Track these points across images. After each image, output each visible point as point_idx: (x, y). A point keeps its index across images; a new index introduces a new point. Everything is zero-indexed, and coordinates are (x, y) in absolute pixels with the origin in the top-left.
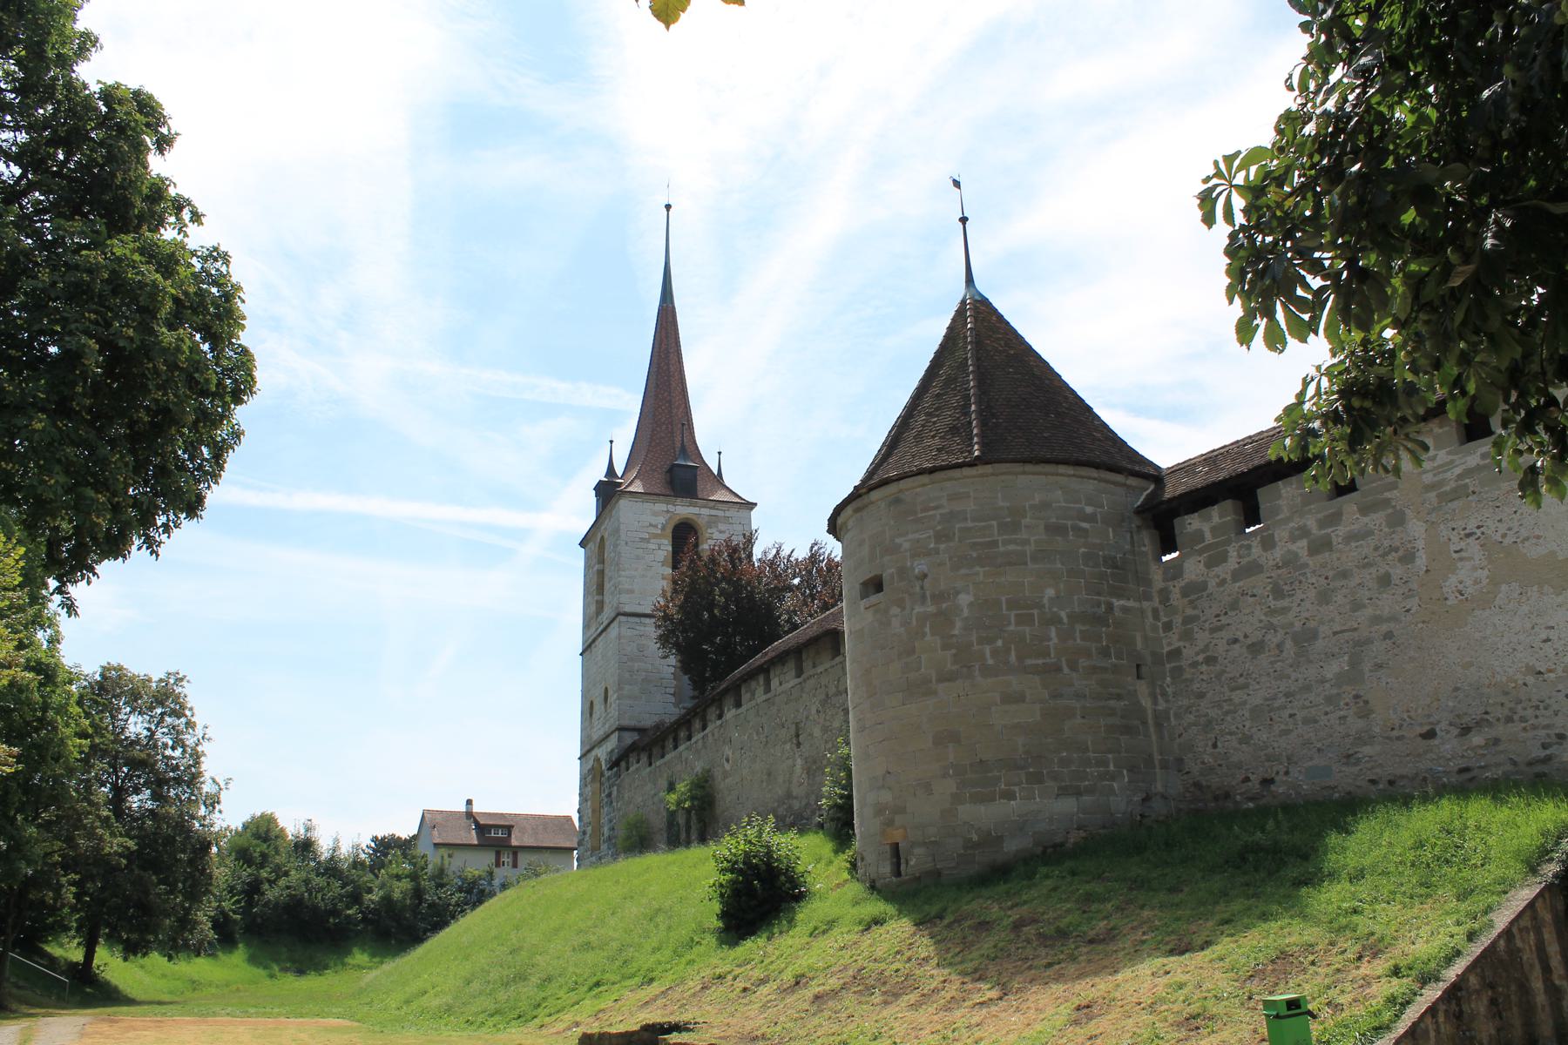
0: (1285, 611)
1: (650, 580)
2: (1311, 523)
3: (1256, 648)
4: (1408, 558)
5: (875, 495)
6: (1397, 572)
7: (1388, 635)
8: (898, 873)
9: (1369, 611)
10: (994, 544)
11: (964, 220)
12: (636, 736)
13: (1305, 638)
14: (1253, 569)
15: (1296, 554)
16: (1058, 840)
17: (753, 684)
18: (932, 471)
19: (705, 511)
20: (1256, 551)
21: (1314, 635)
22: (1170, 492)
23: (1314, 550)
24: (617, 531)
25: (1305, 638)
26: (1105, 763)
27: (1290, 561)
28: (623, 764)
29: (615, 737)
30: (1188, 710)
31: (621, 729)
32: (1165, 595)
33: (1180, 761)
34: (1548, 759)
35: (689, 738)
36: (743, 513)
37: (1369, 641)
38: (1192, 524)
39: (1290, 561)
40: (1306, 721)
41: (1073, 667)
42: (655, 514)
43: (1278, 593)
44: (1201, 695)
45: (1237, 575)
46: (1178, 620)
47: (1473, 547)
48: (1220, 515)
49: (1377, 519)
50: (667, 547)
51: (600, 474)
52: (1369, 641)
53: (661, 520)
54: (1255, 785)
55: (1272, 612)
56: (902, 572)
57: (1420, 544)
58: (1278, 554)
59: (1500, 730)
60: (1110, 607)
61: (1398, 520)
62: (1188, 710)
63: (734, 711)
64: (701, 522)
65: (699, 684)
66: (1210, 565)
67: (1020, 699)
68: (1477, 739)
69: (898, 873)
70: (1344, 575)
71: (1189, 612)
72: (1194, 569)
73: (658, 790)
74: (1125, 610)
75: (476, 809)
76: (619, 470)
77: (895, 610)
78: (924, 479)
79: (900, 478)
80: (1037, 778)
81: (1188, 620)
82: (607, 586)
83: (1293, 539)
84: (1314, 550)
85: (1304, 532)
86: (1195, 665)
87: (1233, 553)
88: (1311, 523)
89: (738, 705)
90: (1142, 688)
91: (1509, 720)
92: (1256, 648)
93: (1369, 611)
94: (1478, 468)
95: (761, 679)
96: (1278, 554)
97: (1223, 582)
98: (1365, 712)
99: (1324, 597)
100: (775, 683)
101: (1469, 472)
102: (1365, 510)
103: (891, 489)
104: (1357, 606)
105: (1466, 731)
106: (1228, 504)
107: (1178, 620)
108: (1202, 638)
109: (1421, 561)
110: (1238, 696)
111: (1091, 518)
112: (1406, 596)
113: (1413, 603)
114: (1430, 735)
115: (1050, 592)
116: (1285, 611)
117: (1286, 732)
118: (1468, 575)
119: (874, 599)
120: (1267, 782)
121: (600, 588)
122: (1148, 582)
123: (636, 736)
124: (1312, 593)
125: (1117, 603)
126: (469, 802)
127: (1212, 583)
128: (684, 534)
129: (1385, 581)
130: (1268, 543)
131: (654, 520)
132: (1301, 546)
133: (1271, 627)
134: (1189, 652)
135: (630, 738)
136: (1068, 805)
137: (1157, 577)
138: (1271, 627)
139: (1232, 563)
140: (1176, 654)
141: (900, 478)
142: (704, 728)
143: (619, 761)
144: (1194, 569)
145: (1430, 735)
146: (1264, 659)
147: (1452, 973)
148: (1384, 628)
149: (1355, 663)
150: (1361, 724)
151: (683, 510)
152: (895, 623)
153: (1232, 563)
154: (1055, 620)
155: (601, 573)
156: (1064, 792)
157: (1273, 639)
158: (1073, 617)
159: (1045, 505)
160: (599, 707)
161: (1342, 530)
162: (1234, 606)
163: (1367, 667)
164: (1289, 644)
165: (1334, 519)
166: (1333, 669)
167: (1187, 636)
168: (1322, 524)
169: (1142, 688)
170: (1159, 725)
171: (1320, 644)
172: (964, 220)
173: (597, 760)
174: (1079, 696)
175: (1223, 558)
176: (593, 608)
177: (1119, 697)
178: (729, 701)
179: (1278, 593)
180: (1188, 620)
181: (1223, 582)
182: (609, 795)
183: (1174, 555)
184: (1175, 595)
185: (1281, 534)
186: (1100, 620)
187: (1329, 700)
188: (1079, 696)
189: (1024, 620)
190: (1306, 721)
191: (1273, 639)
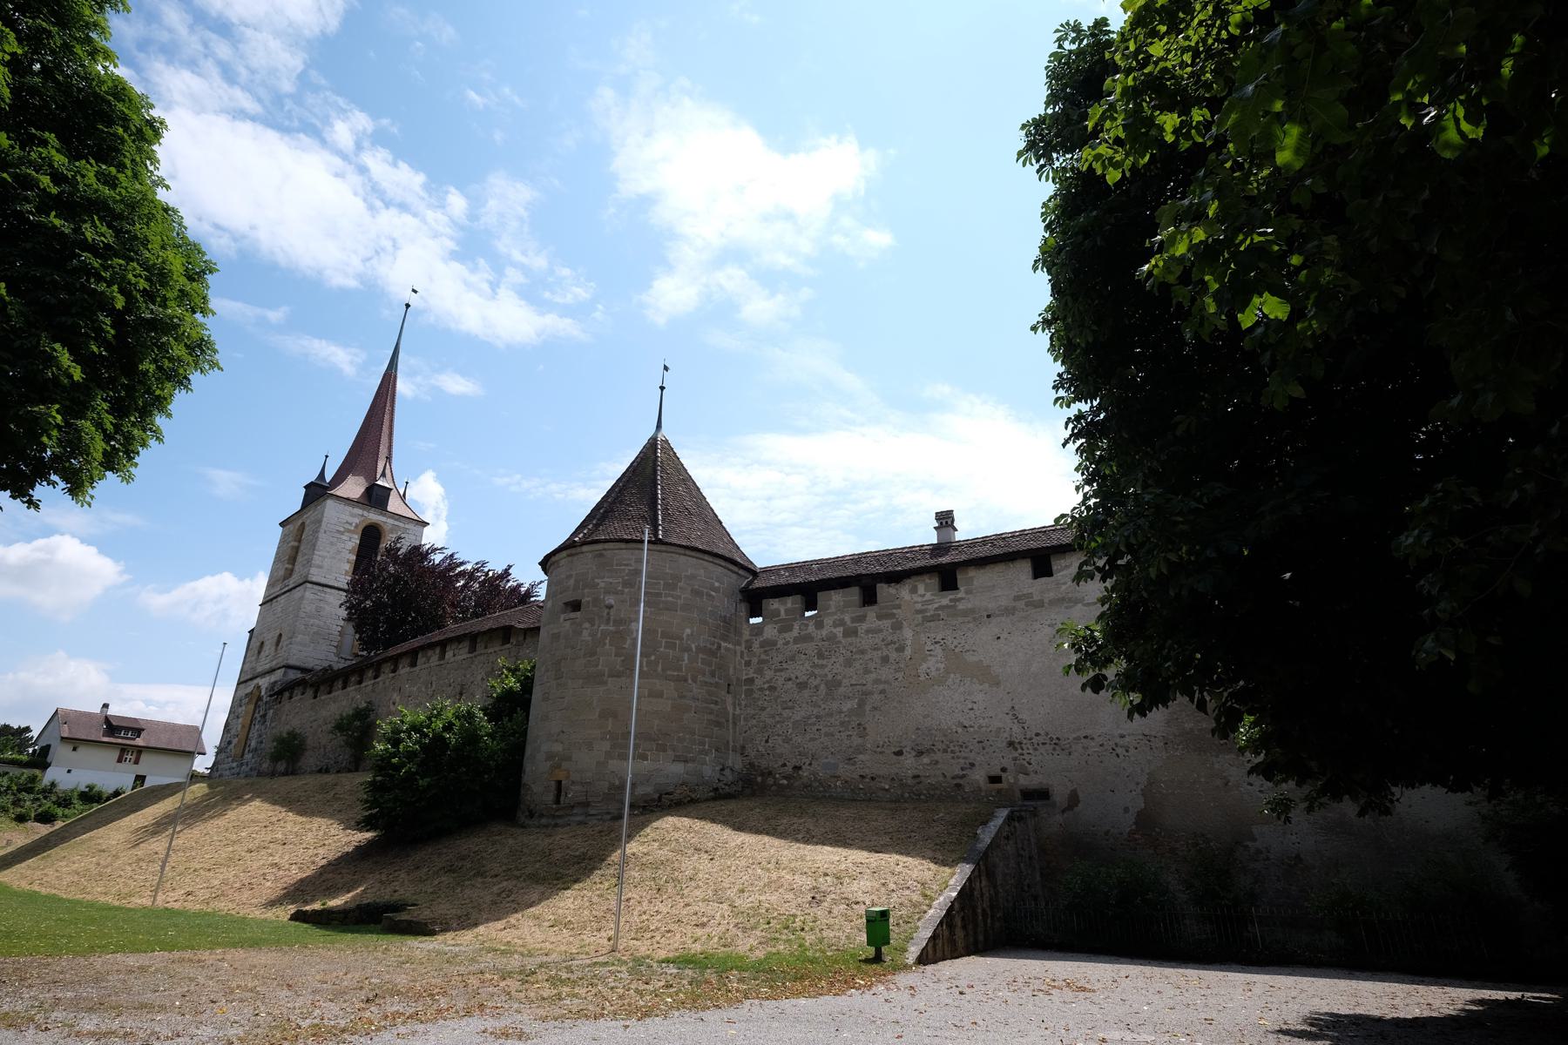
0: (823, 666)
1: (335, 561)
2: (847, 618)
3: (802, 686)
4: (901, 649)
5: (585, 548)
6: (893, 655)
7: (882, 692)
8: (557, 801)
9: (873, 676)
10: (659, 595)
11: (662, 388)
12: (299, 675)
13: (833, 684)
14: (808, 638)
15: (835, 636)
16: (670, 789)
17: (430, 653)
18: (627, 541)
19: (390, 521)
20: (811, 628)
21: (839, 684)
22: (758, 584)
23: (847, 634)
24: (320, 521)
25: (833, 684)
26: (703, 744)
27: (831, 638)
28: (287, 694)
29: (279, 673)
30: (753, 717)
31: (288, 667)
32: (749, 647)
33: (743, 748)
34: (964, 776)
35: (360, 682)
36: (418, 528)
37: (871, 693)
38: (774, 604)
39: (831, 638)
40: (826, 735)
41: (694, 680)
42: (353, 515)
43: (820, 655)
44: (763, 709)
45: (796, 641)
46: (755, 660)
47: (938, 650)
48: (792, 602)
49: (887, 623)
50: (356, 540)
51: (313, 478)
52: (871, 693)
53: (357, 520)
54: (789, 769)
55: (815, 666)
56: (596, 601)
57: (909, 642)
58: (824, 632)
59: (938, 756)
60: (719, 647)
61: (897, 627)
62: (753, 717)
63: (408, 669)
64: (387, 528)
65: (367, 643)
66: (780, 632)
67: (660, 695)
68: (926, 760)
69: (557, 801)
70: (863, 652)
71: (763, 657)
72: (770, 632)
73: (313, 718)
74: (727, 649)
75: (112, 711)
76: (329, 477)
77: (587, 625)
78: (623, 545)
79: (606, 541)
80: (663, 748)
81: (761, 662)
82: (299, 559)
83: (835, 625)
84: (847, 634)
85: (842, 623)
86: (761, 689)
87: (796, 627)
88: (847, 618)
89: (413, 664)
90: (729, 699)
91: (945, 751)
92: (802, 686)
93: (873, 676)
94: (947, 607)
95: (438, 650)
96: (824, 632)
97: (787, 643)
98: (862, 730)
99: (848, 663)
100: (449, 654)
101: (941, 608)
102: (879, 617)
103: (600, 546)
104: (867, 671)
105: (920, 753)
106: (798, 597)
107: (755, 660)
108: (769, 674)
109: (908, 652)
110: (786, 713)
111: (716, 590)
112: (896, 671)
113: (900, 675)
114: (899, 753)
115: (688, 631)
116: (823, 666)
117: (812, 740)
118: (934, 664)
119: (573, 615)
120: (797, 768)
121: (293, 560)
122: (740, 635)
123: (299, 675)
124: (841, 659)
125: (723, 644)
126: (106, 706)
127: (780, 642)
128: (371, 535)
129: (885, 660)
130: (819, 624)
131: (350, 519)
132: (839, 631)
133: (813, 675)
134: (759, 682)
135: (297, 675)
136: (678, 769)
137: (746, 634)
138: (813, 675)
139: (795, 633)
140: (751, 681)
141: (606, 541)
142: (376, 677)
143: (280, 692)
144: (770, 632)
145: (899, 753)
146: (806, 693)
147: (188, 954)
148: (881, 687)
149: (861, 704)
150: (860, 741)
151: (374, 517)
152: (585, 633)
153: (795, 633)
154: (688, 649)
155: (297, 549)
156: (677, 759)
157: (814, 682)
158: (699, 650)
159: (693, 577)
160: (269, 649)
161: (864, 626)
162: (793, 659)
163: (868, 708)
164: (823, 687)
165: (862, 619)
166: (848, 706)
167: (760, 671)
168: (854, 620)
169: (729, 699)
170: (735, 724)
171: (842, 689)
172: (662, 388)
173: (258, 687)
174: (695, 699)
175: (790, 629)
176: (282, 573)
177: (716, 703)
178: (405, 661)
179: (820, 655)
180: (761, 662)
181: (787, 643)
182: (264, 716)
183: (760, 620)
184: (756, 645)
185: (828, 621)
186: (713, 653)
187: (842, 723)
188: (695, 699)
189: (671, 646)
190: (826, 735)
191: (814, 682)
